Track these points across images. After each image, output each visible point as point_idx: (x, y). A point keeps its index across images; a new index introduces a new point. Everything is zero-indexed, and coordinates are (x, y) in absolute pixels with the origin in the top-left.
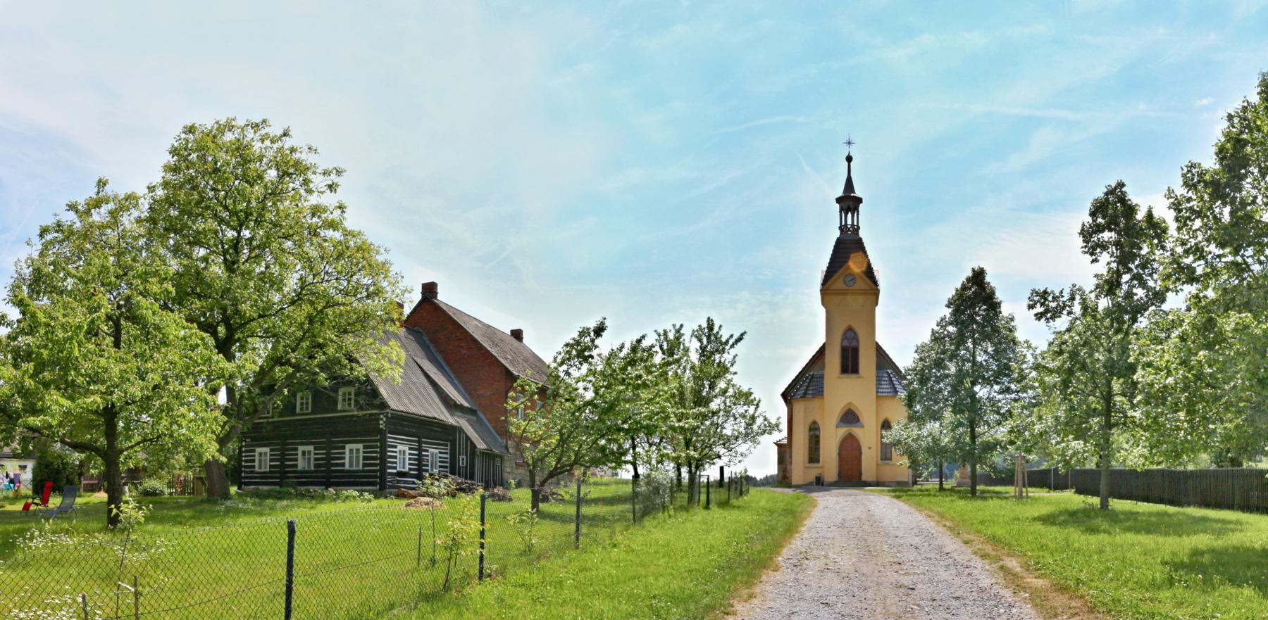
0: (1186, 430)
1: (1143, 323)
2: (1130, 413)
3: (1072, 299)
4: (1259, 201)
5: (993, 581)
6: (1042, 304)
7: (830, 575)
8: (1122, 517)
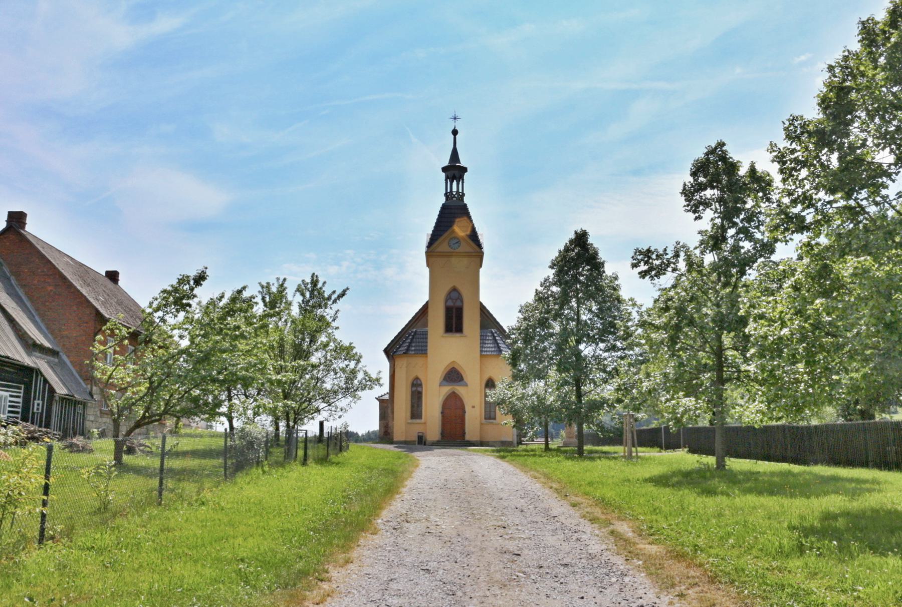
0: (806, 382)
1: (752, 275)
2: (743, 367)
3: (677, 255)
4: (869, 142)
5: (604, 547)
6: (646, 263)
7: (431, 539)
8: (740, 477)
